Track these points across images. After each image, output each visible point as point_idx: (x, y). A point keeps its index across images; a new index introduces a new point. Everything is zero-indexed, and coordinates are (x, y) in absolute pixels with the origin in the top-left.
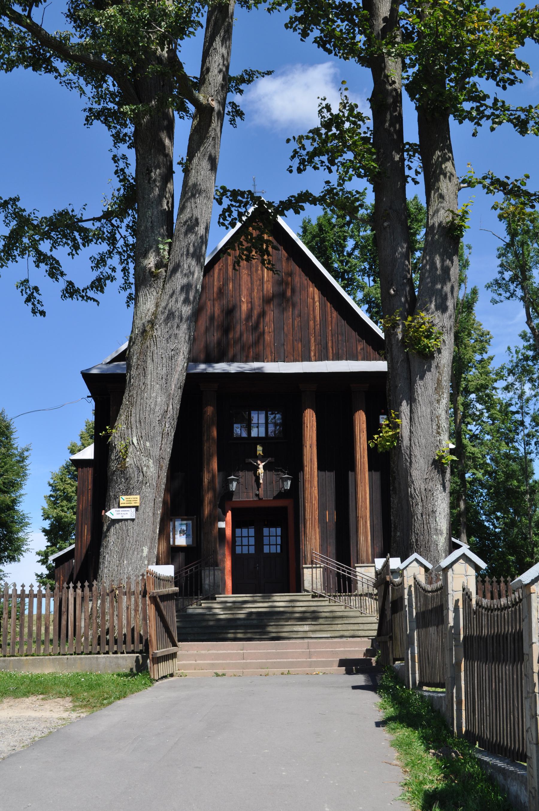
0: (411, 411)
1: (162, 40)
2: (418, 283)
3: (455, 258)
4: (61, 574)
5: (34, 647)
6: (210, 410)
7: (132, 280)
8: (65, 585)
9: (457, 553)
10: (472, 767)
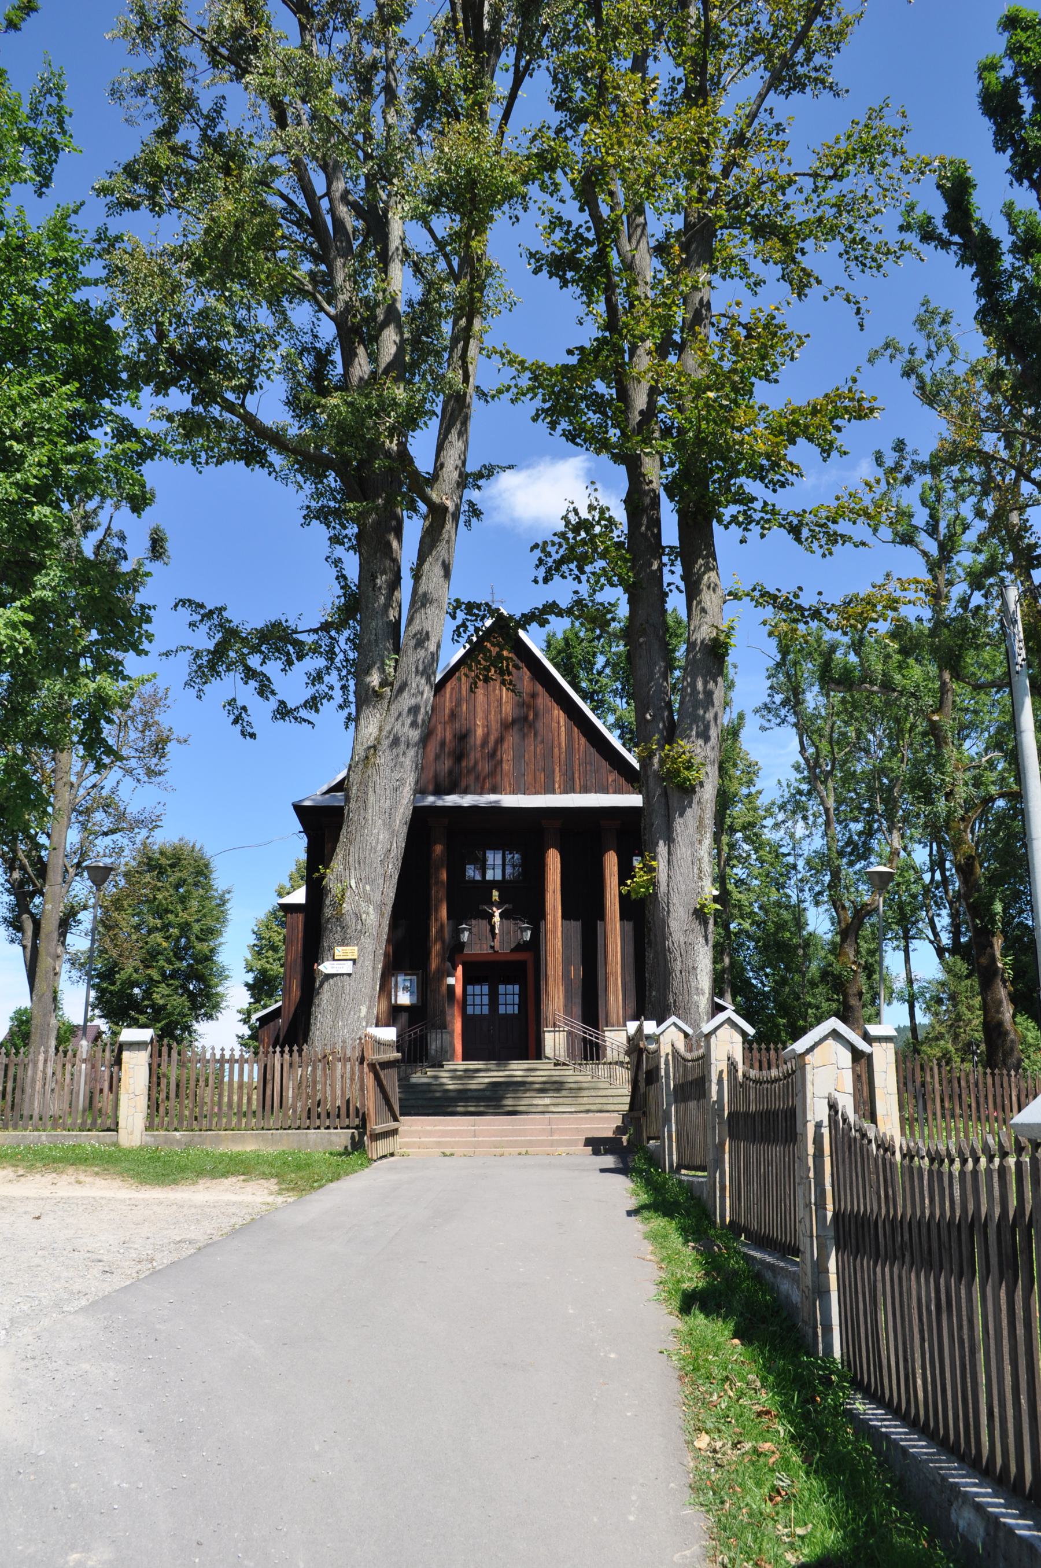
0: (669, 853)
1: (392, 431)
2: (677, 706)
3: (720, 679)
4: (267, 1035)
5: (234, 1120)
6: (438, 849)
7: (352, 698)
8: (271, 1049)
9: (721, 1017)
10: (737, 1263)
